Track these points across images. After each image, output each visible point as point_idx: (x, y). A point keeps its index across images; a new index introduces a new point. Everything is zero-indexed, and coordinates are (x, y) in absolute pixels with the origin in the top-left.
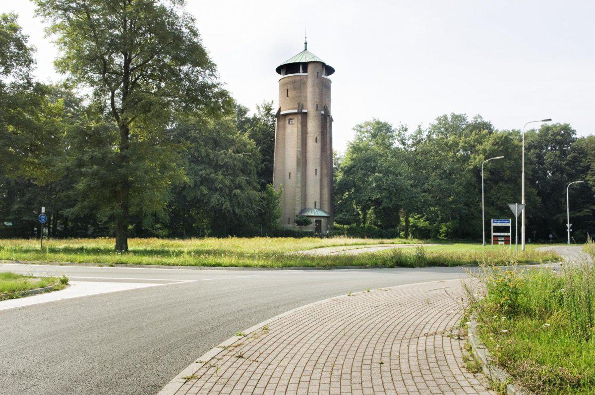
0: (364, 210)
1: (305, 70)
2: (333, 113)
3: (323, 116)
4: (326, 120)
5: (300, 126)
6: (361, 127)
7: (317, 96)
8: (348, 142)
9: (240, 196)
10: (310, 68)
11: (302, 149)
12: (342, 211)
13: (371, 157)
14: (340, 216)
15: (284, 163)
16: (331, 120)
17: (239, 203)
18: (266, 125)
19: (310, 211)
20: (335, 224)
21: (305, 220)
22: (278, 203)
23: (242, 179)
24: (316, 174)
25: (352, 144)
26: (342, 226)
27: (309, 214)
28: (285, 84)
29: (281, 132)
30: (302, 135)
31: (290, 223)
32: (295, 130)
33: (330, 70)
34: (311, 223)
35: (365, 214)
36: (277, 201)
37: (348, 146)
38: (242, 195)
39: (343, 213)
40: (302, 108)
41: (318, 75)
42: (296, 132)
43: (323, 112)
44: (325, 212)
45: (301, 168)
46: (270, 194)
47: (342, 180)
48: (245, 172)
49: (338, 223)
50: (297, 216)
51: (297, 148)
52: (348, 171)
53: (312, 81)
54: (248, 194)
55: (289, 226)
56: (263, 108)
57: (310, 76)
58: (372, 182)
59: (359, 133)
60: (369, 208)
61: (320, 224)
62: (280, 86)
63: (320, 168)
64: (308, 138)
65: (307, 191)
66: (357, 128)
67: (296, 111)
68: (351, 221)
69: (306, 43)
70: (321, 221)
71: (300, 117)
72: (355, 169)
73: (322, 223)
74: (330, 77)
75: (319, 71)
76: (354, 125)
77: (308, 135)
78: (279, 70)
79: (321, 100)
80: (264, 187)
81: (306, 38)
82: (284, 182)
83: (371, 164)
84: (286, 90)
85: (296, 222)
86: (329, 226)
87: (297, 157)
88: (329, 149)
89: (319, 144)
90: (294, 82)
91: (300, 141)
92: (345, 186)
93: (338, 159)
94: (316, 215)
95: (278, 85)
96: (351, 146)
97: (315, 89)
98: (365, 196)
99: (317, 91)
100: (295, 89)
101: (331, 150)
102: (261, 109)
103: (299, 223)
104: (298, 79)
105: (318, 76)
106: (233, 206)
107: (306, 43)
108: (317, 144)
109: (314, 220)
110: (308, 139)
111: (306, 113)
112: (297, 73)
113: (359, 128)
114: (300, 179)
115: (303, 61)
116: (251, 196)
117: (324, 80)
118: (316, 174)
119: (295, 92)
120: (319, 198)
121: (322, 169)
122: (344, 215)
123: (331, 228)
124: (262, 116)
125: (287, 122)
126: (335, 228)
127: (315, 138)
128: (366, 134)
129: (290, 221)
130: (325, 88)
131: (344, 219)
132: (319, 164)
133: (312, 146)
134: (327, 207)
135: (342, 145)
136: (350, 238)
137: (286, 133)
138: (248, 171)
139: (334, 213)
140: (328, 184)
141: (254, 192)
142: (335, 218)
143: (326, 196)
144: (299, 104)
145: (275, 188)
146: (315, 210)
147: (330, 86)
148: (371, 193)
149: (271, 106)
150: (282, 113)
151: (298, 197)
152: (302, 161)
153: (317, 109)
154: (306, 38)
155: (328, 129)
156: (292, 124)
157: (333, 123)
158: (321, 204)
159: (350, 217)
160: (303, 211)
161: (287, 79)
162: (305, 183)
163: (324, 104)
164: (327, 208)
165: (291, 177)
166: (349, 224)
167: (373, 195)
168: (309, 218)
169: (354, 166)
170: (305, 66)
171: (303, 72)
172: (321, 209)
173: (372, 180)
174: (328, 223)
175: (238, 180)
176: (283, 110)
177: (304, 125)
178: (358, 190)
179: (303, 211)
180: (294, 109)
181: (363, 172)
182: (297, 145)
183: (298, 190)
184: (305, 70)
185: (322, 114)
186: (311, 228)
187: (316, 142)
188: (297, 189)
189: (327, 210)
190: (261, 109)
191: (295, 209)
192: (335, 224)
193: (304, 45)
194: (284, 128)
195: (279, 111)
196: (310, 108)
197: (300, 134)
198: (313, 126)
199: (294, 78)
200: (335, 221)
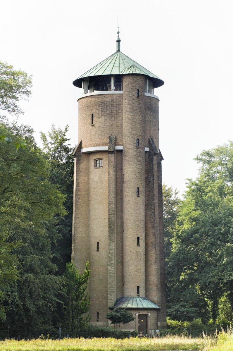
0: (214, 298)
1: (119, 86)
2: (163, 147)
3: (147, 154)
4: (152, 160)
5: (112, 171)
6: (210, 155)
7: (138, 125)
8: (188, 182)
9: (33, 283)
10: (126, 82)
11: (117, 207)
12: (179, 301)
13: (220, 218)
14: (176, 307)
15: (88, 227)
16: (161, 158)
17: (31, 294)
18: (58, 166)
19: (131, 302)
20: (169, 321)
21: (124, 315)
22: (84, 290)
23: (34, 258)
24: (138, 244)
25: (196, 185)
26: (179, 323)
27: (129, 306)
28: (88, 106)
29: (83, 179)
30: (116, 183)
31: (99, 320)
32: (106, 176)
33: (157, 83)
34: (133, 319)
35: (216, 304)
36: (82, 287)
37: (188, 187)
38: (38, 281)
39: (181, 303)
40: (116, 144)
41: (138, 93)
42: (107, 179)
43: (147, 149)
44: (154, 303)
45: (115, 235)
46: (72, 277)
47: (181, 251)
48: (36, 247)
49: (173, 319)
50: (111, 309)
51: (109, 204)
52: (187, 239)
53: (130, 104)
54: (44, 280)
55: (98, 324)
56: (52, 138)
57: (125, 94)
58: (221, 256)
59: (207, 166)
60: (220, 295)
61: (146, 321)
62: (80, 109)
63: (143, 234)
64: (124, 189)
65: (125, 271)
66: (204, 158)
67: (106, 148)
68: (193, 315)
69: (119, 41)
70: (146, 316)
71: (112, 157)
72: (197, 235)
73: (149, 319)
74: (157, 92)
75: (140, 89)
76: (198, 152)
77: (125, 185)
78: (78, 83)
79: (144, 130)
80: (62, 270)
81: (118, 33)
82: (89, 257)
83: (220, 229)
84: (91, 114)
85: (110, 318)
86: (159, 324)
87: (109, 219)
88: (156, 184)
89: (142, 199)
90: (102, 104)
91: (113, 195)
92: (182, 261)
93: (174, 203)
94: (140, 306)
95: (76, 106)
96: (193, 187)
97: (134, 116)
98: (211, 276)
99: (138, 117)
100: (104, 114)
101: (160, 187)
102: (49, 140)
103: (115, 320)
104: (107, 99)
105: (139, 95)
106: (22, 298)
107: (119, 41)
108: (139, 199)
109: (137, 315)
110: (124, 192)
111: (121, 151)
112: (107, 90)
113: (207, 158)
114: (114, 252)
115: (116, 72)
116: (49, 283)
117: (148, 101)
118: (138, 244)
119: (104, 119)
120: (144, 280)
121: (146, 236)
122: (181, 306)
123: (163, 327)
124: (50, 150)
125: (92, 163)
126: (169, 327)
127: (136, 189)
128: (219, 168)
129: (100, 317)
130: (149, 110)
131: (182, 312)
132: (143, 230)
133: (131, 202)
134: (155, 295)
135: (179, 176)
136: (188, 337)
137: (91, 181)
138: (40, 245)
139: (168, 301)
140: (156, 258)
141: (52, 276)
142: (169, 310)
143: (154, 277)
144: (110, 137)
145: (77, 266)
146: (138, 299)
147: (158, 107)
148: (222, 272)
149: (64, 135)
150: (84, 150)
151: (113, 280)
152: (117, 226)
153: (138, 146)
154: (118, 33)
155: (155, 174)
156: (100, 167)
157: (163, 162)
158: (147, 289)
159: (190, 309)
160: (119, 301)
161: (90, 99)
162: (122, 257)
163: (148, 136)
164: (156, 295)
165: (100, 250)
166: (190, 319)
167: (224, 276)
168: (131, 312)
169: (196, 231)
170: (119, 79)
171: (115, 90)
172: (147, 297)
173: (222, 253)
174: (157, 319)
175: (29, 259)
176: (86, 147)
177: (119, 169)
178: (204, 267)
179: (119, 301)
180: (103, 145)
181: (210, 240)
182: (109, 201)
183: (112, 270)
184: (119, 86)
185: (146, 152)
186: (133, 326)
187: (138, 195)
188: (109, 268)
189: (155, 299)
190: (49, 140)
191: (106, 299)
192: (169, 321)
193: (116, 44)
194: (88, 174)
195: (80, 146)
196: (127, 144)
197: (113, 187)
198: (132, 171)
199: (102, 99)
200: (169, 315)
